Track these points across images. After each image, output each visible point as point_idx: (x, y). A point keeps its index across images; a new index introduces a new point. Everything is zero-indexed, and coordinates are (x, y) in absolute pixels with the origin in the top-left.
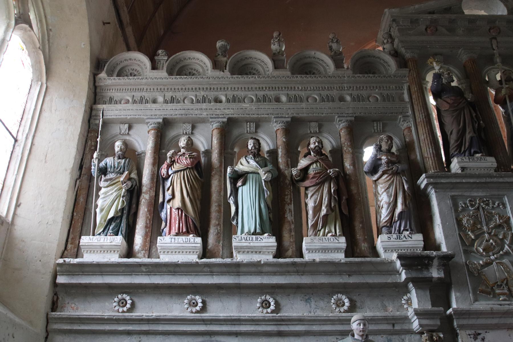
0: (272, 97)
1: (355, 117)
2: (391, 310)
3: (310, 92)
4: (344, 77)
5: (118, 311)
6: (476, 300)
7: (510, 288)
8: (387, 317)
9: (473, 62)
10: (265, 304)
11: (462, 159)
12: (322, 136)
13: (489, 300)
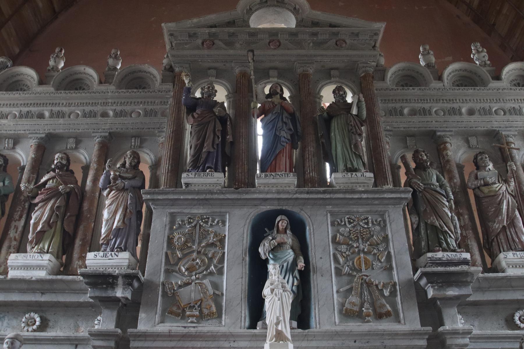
0: (35, 113)
1: (110, 133)
2: (82, 330)
3: (74, 108)
4: (108, 92)
5: (28, 331)
6: (162, 322)
7: (202, 309)
8: (70, 338)
9: (243, 76)
10: (31, 322)
11: (187, 175)
12: (79, 152)
13: (177, 322)
